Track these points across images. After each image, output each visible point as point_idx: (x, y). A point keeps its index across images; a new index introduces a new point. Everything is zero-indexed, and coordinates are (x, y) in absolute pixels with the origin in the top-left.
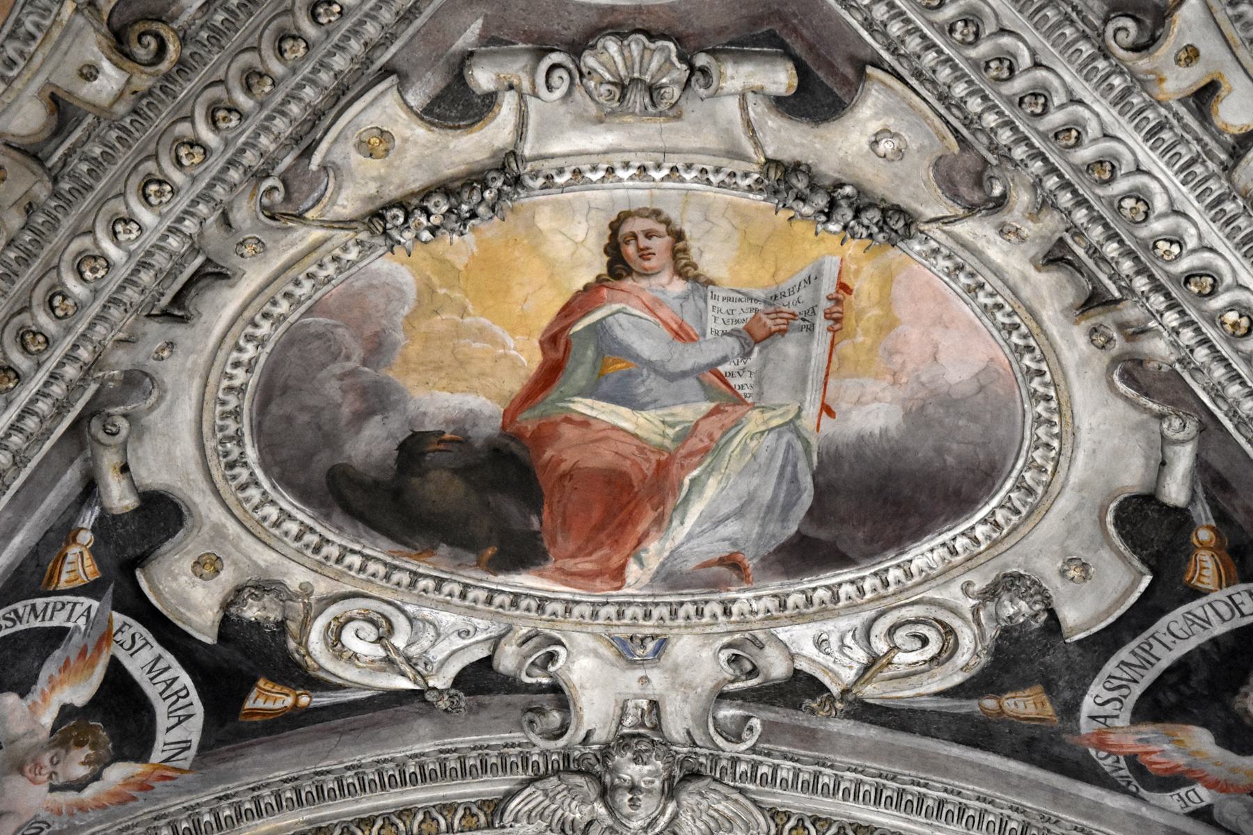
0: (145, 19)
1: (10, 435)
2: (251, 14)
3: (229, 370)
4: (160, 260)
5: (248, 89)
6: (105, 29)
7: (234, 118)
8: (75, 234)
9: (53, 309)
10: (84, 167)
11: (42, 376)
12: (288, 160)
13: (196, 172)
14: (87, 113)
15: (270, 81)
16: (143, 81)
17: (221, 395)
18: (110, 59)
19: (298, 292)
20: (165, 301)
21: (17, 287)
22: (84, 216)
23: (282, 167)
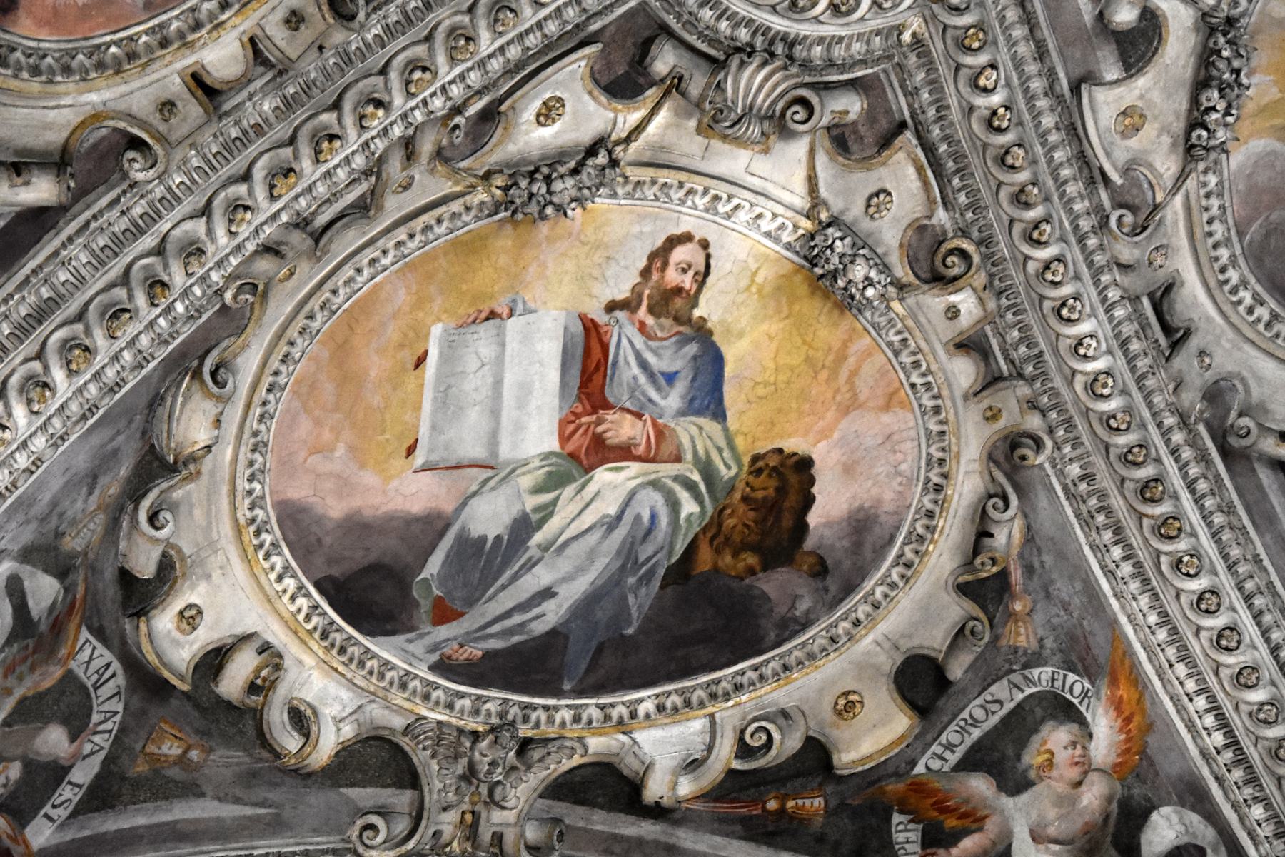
0: (935, 253)
1: (1203, 505)
2: (973, 174)
3: (1251, 319)
4: (1128, 329)
5: (1028, 206)
6: (926, 287)
7: (1044, 226)
8: (1070, 382)
9: (1118, 429)
10: (1022, 349)
11: (1168, 461)
12: (1104, 196)
13: (1071, 273)
14: (983, 328)
15: (1030, 187)
16: (980, 279)
17: (1268, 334)
18: (951, 293)
19: (1218, 236)
20: (1163, 341)
21: (1087, 443)
22: (1060, 369)
23: (1107, 203)
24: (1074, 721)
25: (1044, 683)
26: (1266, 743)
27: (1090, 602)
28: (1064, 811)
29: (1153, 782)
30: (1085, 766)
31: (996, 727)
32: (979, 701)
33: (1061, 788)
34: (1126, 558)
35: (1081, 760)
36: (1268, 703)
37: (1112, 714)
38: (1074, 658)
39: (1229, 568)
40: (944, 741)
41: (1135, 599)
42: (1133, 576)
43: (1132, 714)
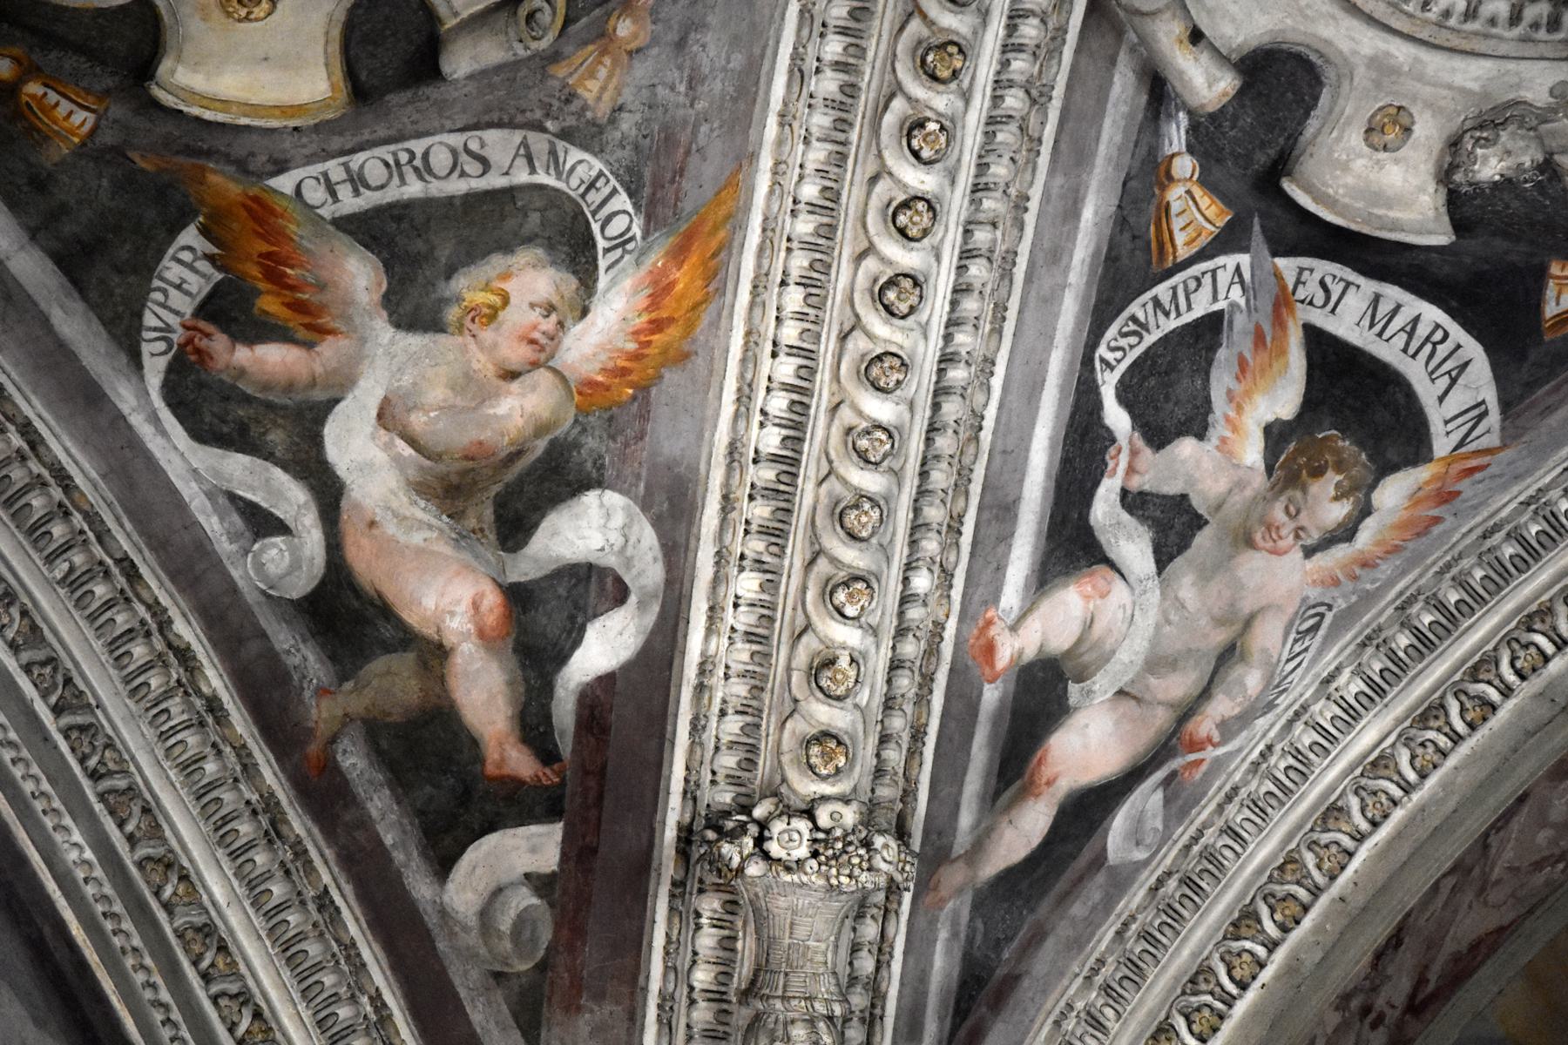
24: (575, 273)
25: (574, 182)
26: (838, 488)
27: (734, 100)
28: (459, 402)
29: (627, 445)
30: (542, 353)
31: (450, 199)
32: (456, 140)
33: (482, 363)
34: (839, 66)
35: (543, 340)
36: (885, 429)
37: (642, 300)
38: (647, 173)
39: (976, 189)
40: (354, 166)
41: (806, 141)
42: (829, 103)
43: (671, 320)
